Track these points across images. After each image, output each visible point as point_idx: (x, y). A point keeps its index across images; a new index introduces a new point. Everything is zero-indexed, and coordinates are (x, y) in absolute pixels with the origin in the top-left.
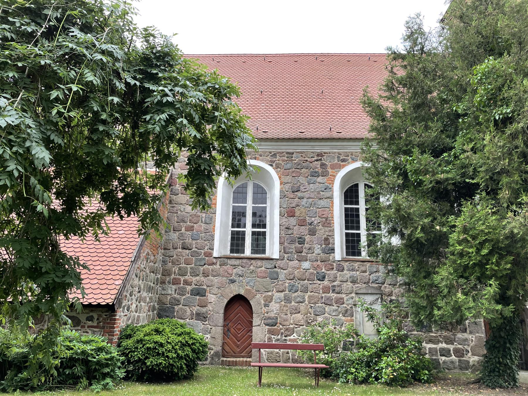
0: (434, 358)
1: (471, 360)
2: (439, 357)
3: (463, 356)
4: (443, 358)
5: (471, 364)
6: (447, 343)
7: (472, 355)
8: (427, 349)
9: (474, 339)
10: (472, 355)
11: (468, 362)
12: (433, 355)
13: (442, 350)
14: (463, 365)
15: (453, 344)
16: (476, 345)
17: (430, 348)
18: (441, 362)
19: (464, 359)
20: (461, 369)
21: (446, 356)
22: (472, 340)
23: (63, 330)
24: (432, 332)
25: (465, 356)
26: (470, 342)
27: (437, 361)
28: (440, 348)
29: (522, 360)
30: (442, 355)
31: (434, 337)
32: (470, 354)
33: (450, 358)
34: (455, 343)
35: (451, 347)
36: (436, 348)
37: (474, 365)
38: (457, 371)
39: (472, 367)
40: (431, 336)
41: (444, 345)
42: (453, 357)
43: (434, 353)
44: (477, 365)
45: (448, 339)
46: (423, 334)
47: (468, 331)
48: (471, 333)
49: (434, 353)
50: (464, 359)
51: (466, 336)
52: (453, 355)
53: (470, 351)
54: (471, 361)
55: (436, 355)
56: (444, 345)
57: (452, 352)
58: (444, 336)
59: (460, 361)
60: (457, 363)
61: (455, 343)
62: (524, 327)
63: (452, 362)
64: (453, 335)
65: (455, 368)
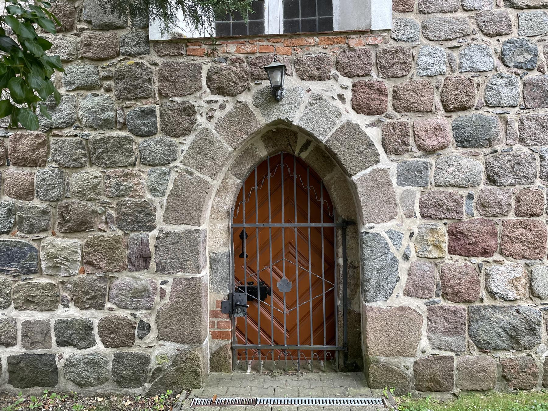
0: (38, 351)
1: (154, 354)
2: (55, 348)
3: (129, 340)
4: (68, 352)
5: (153, 365)
6: (81, 304)
7: (159, 338)
8: (19, 327)
9: (168, 288)
10: (159, 338)
11: (146, 360)
12: (34, 344)
13: (64, 326)
14: (127, 372)
15: (101, 307)
16: (172, 308)
17: (27, 324)
18: (60, 364)
19: (134, 350)
20: (118, 383)
21: (75, 346)
22: (163, 293)
23: (84, 120)
24: (38, 272)
25: (137, 341)
26: (157, 298)
27: (49, 361)
28: (59, 322)
29: (331, 340)
30: (61, 343)
31: (43, 287)
32: (153, 335)
33: (90, 350)
34: (108, 305)
35: (95, 317)
36: (46, 323)
37: (159, 370)
38: (108, 387)
39: (153, 377)
40: (35, 286)
41: (73, 312)
42: (100, 347)
43: (39, 338)
44: (172, 370)
45: (86, 293)
46: (10, 279)
47: (153, 265)
48: (160, 269)
49: (39, 338)
50: (130, 351)
51: (144, 278)
52: (98, 339)
53: (153, 326)
54: (153, 358)
55: (45, 342)
56: (73, 312)
57: (96, 332)
58: (76, 285)
59: (118, 357)
60: (110, 366)
61: (108, 305)
62: (350, 242)
63: (93, 363)
64: (103, 279)
65: (100, 381)
